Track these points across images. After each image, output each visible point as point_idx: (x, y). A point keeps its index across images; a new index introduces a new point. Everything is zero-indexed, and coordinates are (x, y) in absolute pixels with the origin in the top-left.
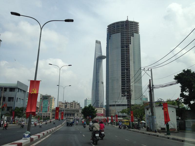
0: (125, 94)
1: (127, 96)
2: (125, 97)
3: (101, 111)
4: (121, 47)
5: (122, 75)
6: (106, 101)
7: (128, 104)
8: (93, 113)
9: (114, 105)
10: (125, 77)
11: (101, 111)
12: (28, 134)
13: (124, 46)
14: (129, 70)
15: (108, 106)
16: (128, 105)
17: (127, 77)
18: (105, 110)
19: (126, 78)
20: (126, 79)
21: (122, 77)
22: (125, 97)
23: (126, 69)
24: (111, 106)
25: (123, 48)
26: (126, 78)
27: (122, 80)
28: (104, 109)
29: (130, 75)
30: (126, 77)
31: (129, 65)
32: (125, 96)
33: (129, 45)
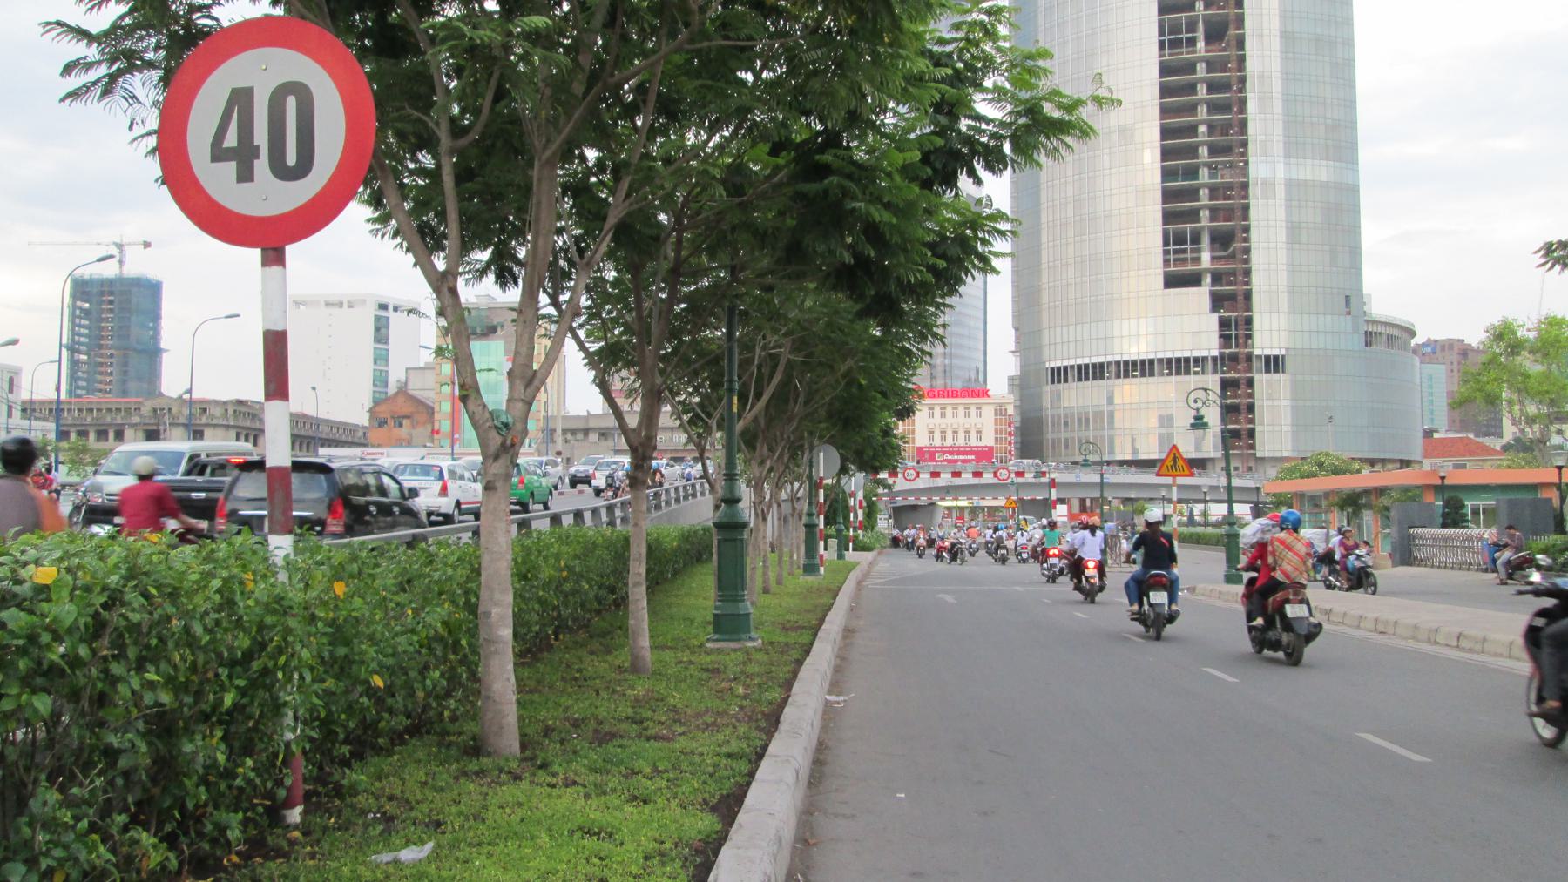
0: (1197, 260)
1: (1217, 278)
2: (1199, 296)
3: (973, 420)
4: (1155, 40)
5: (1165, 91)
6: (1018, 340)
7: (1222, 356)
8: (970, 90)
9: (1092, 372)
10: (1192, 108)
11: (973, 420)
12: (220, 670)
13: (1192, 27)
14: (1232, 32)
15: (1023, 385)
16: (1222, 362)
17: (1214, 107)
18: (1011, 410)
19: (1202, 113)
20: (1202, 129)
21: (1165, 111)
22: (1199, 296)
23: (1201, 27)
24: (1059, 375)
25: (1175, 44)
26: (1202, 113)
27: (1166, 133)
28: (1000, 410)
29: (1243, 80)
30: (1209, 166)
31: (1234, 52)
32: (1193, 280)
33: (1250, 383)
